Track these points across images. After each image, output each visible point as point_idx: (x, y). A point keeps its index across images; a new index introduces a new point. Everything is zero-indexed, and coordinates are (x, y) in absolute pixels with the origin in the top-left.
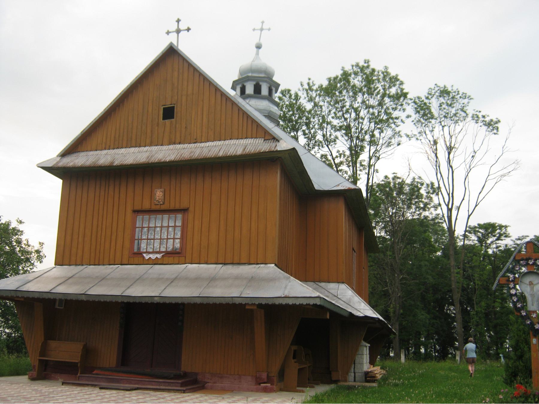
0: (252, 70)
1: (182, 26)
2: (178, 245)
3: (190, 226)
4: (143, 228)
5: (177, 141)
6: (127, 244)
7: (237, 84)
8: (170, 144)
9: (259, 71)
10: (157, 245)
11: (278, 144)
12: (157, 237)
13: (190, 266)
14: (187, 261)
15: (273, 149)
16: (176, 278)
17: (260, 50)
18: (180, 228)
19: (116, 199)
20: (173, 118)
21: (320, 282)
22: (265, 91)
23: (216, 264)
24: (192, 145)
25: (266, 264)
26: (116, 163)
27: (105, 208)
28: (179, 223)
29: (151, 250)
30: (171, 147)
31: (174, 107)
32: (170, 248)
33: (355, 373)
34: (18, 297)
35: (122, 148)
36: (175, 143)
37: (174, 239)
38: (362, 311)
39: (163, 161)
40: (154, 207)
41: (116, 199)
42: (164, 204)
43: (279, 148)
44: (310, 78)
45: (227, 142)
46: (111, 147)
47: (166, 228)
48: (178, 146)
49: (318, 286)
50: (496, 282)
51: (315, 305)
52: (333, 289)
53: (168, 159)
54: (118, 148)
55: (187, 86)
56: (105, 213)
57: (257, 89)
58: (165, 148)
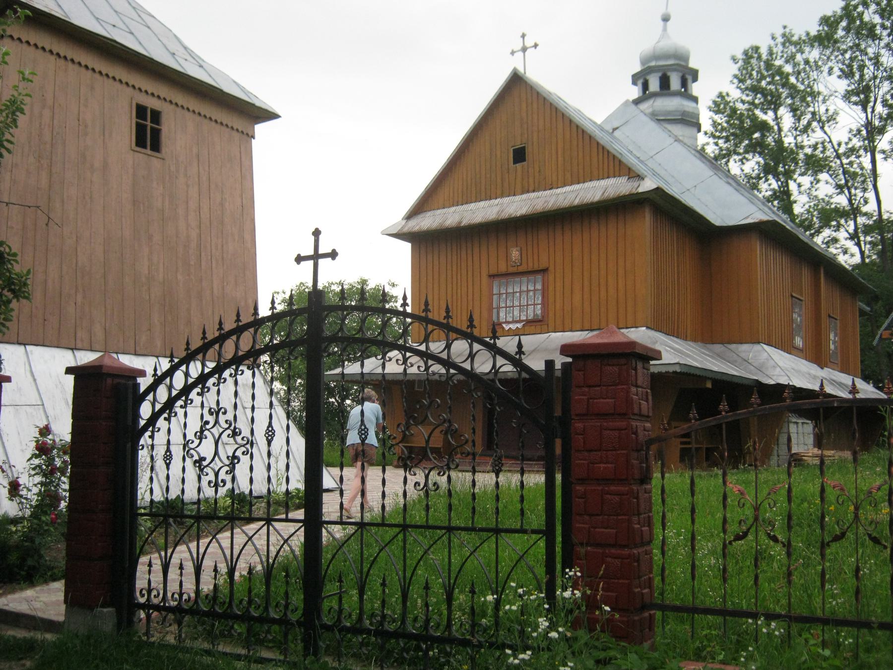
0: (656, 57)
1: (529, 43)
2: (539, 312)
3: (551, 288)
4: (500, 294)
5: (531, 189)
6: (485, 314)
7: (639, 78)
8: (522, 193)
9: (667, 56)
10: (516, 313)
11: (642, 183)
12: (516, 303)
13: (553, 334)
14: (550, 329)
15: (634, 191)
16: (534, 351)
17: (669, 23)
18: (540, 292)
19: (470, 263)
20: (524, 160)
21: (730, 343)
22: (675, 83)
23: (582, 330)
24: (548, 192)
25: (637, 327)
26: (465, 222)
27: (459, 275)
28: (539, 286)
29: (511, 320)
30: (524, 196)
31: (524, 147)
32: (531, 317)
33: (778, 456)
34: (373, 380)
35: (471, 202)
36: (528, 192)
37: (534, 305)
38: (774, 378)
39: (513, 216)
40: (511, 270)
41: (470, 263)
42: (521, 264)
43: (640, 190)
44: (785, 24)
45: (586, 185)
46: (460, 203)
47: (526, 293)
48: (532, 195)
49: (726, 349)
50: (878, 337)
51: (675, 372)
52: (744, 352)
53: (518, 214)
54: (467, 203)
55: (538, 120)
56: (459, 281)
57: (665, 83)
58: (517, 198)
